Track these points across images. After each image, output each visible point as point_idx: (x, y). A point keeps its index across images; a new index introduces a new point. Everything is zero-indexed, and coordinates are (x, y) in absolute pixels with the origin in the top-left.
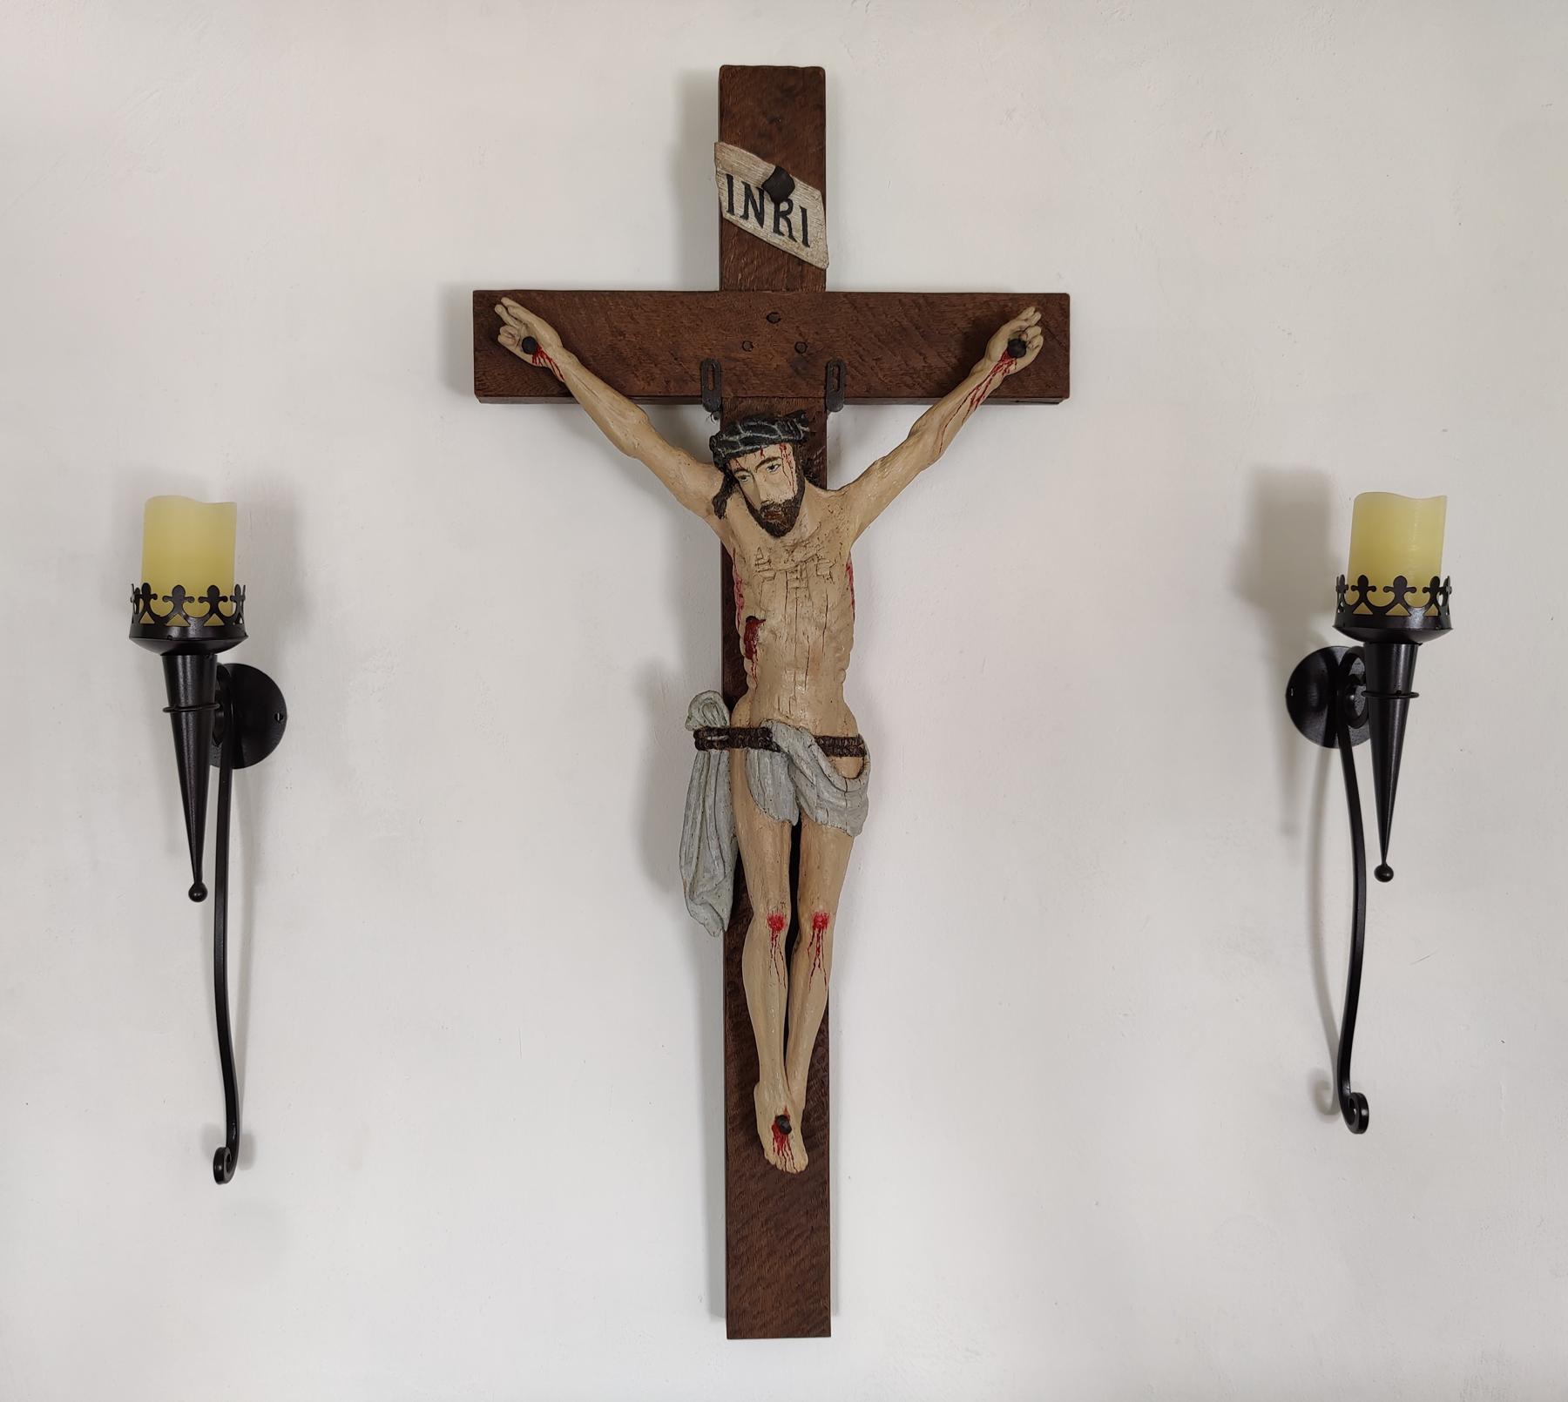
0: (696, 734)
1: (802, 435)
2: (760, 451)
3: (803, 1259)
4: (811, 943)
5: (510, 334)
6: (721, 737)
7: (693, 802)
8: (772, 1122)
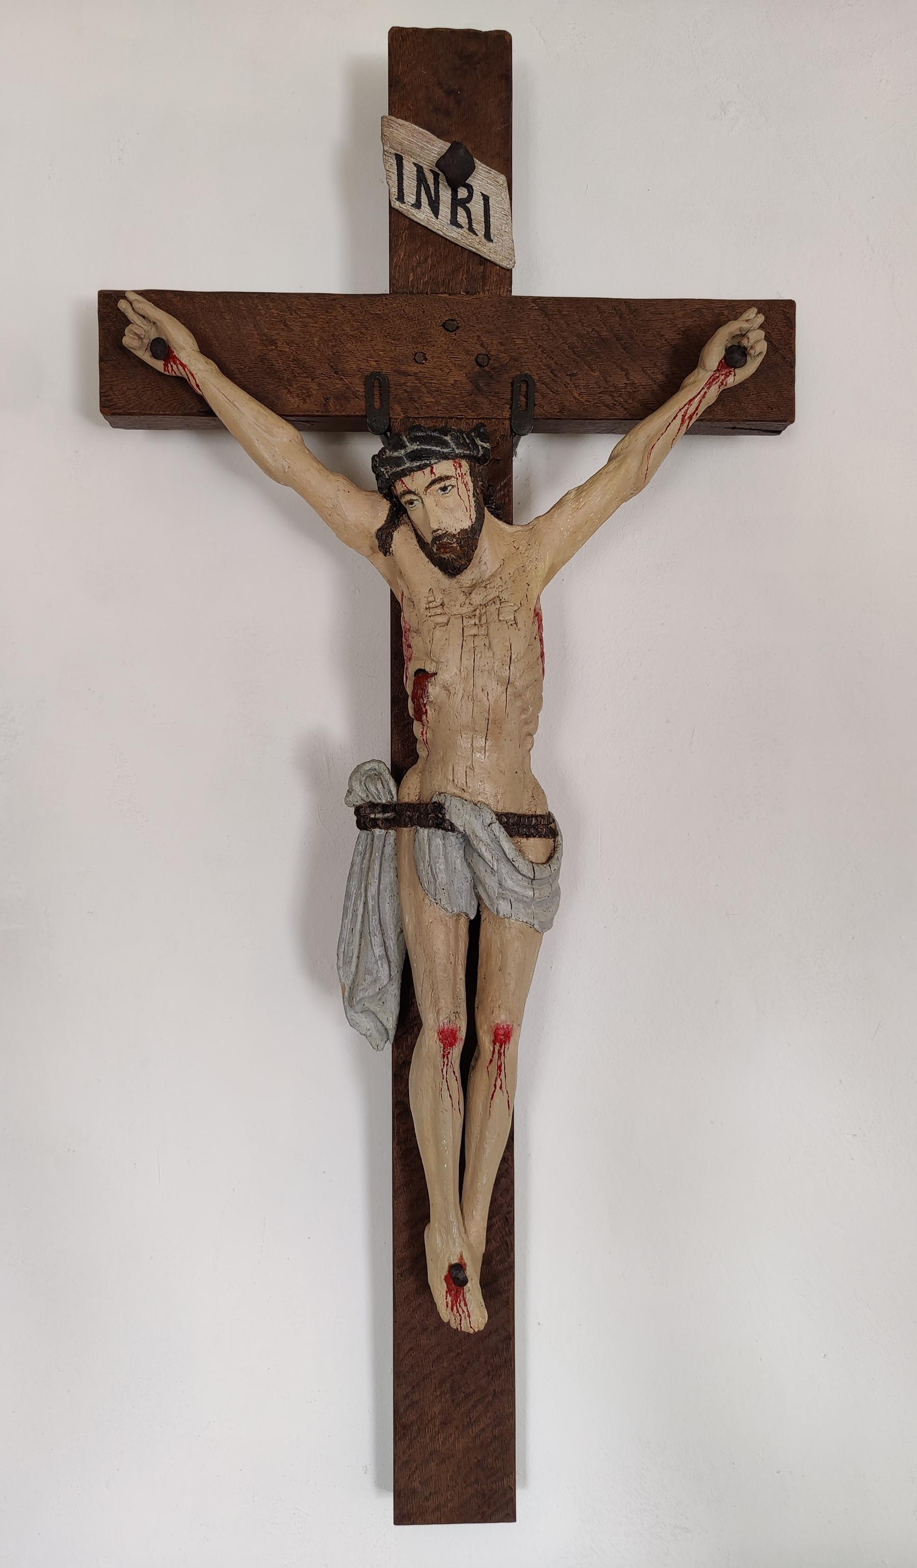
0: (358, 810)
1: (481, 453)
2: (429, 469)
3: (483, 1429)
4: (491, 1061)
5: (136, 334)
6: (387, 815)
7: (353, 891)
8: (445, 1272)
